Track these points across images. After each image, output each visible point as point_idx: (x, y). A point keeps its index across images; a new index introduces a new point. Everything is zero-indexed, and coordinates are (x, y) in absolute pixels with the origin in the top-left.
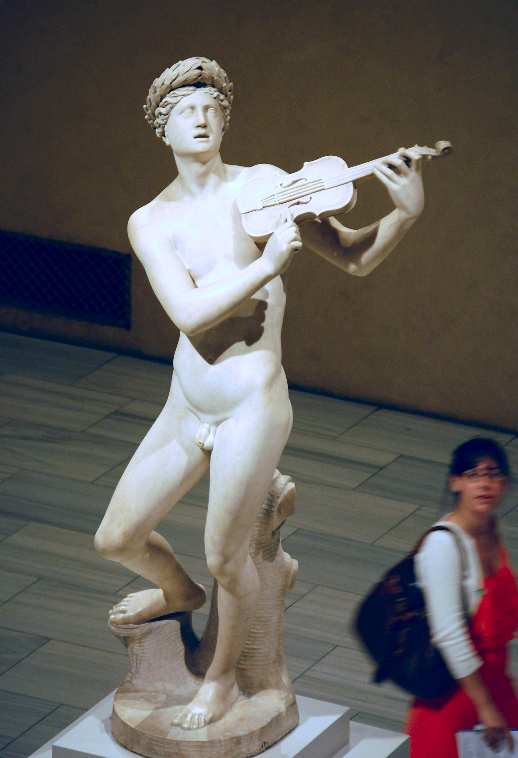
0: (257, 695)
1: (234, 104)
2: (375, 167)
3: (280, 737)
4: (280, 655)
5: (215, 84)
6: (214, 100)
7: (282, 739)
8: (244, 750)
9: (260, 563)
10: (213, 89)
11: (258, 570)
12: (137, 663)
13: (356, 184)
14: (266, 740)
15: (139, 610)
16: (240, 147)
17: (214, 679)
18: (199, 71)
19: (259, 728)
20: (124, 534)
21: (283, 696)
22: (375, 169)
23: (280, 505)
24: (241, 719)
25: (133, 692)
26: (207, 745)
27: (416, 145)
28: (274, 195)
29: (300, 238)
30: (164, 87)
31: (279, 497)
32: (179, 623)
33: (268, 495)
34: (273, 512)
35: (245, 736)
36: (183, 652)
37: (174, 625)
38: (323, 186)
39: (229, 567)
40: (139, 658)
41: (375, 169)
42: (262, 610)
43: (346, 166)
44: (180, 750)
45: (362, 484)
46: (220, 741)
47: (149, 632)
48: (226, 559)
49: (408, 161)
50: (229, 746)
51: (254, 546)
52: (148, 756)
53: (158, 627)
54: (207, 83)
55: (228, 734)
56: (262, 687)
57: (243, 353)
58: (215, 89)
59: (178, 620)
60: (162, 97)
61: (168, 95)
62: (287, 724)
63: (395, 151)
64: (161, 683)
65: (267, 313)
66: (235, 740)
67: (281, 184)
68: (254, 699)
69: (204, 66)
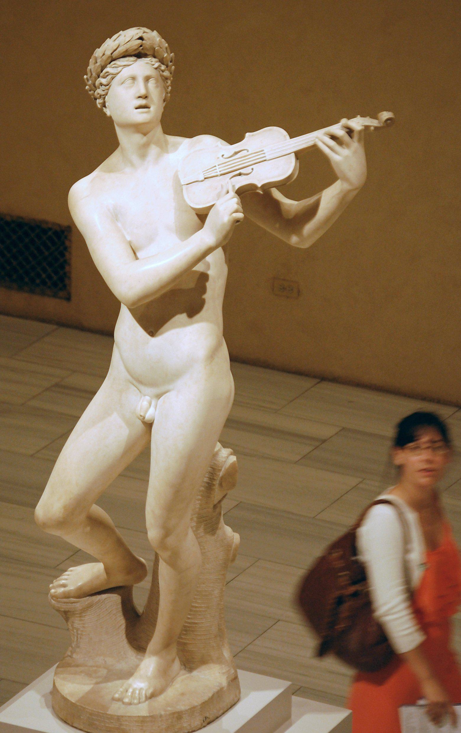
0: (199, 670)
1: (175, 74)
2: (317, 138)
3: (222, 711)
4: (221, 629)
5: (156, 54)
6: (155, 70)
7: (223, 713)
8: (185, 725)
9: (201, 537)
10: (154, 60)
11: (199, 543)
12: (77, 637)
13: (298, 155)
14: (207, 715)
15: (80, 584)
16: (181, 118)
17: (156, 653)
18: (140, 41)
19: (200, 703)
20: (65, 507)
21: (224, 671)
22: (317, 140)
23: (222, 478)
24: (183, 694)
25: (74, 666)
26: (148, 719)
27: (359, 116)
28: (215, 166)
29: (241, 209)
30: (104, 58)
31: (220, 470)
32: (120, 597)
33: (210, 468)
34: (214, 485)
35: (187, 711)
36: (124, 626)
37: (115, 599)
38: (265, 157)
39: (171, 541)
40: (79, 632)
41: (317, 140)
42: (204, 584)
43: (288, 137)
44: (121, 725)
45: (304, 457)
46: (161, 716)
47: (90, 606)
48: (167, 532)
49: (350, 132)
50: (170, 721)
51: (195, 519)
52: (89, 731)
53: (99, 601)
54: (148, 53)
55: (169, 709)
56: (204, 661)
57: (184, 325)
58: (156, 60)
59: (119, 594)
60: (103, 68)
61: (108, 66)
62: (228, 699)
63: (337, 122)
64: (102, 657)
65: (208, 285)
66: (176, 715)
67: (223, 156)
68: (195, 673)
69: (145, 36)
